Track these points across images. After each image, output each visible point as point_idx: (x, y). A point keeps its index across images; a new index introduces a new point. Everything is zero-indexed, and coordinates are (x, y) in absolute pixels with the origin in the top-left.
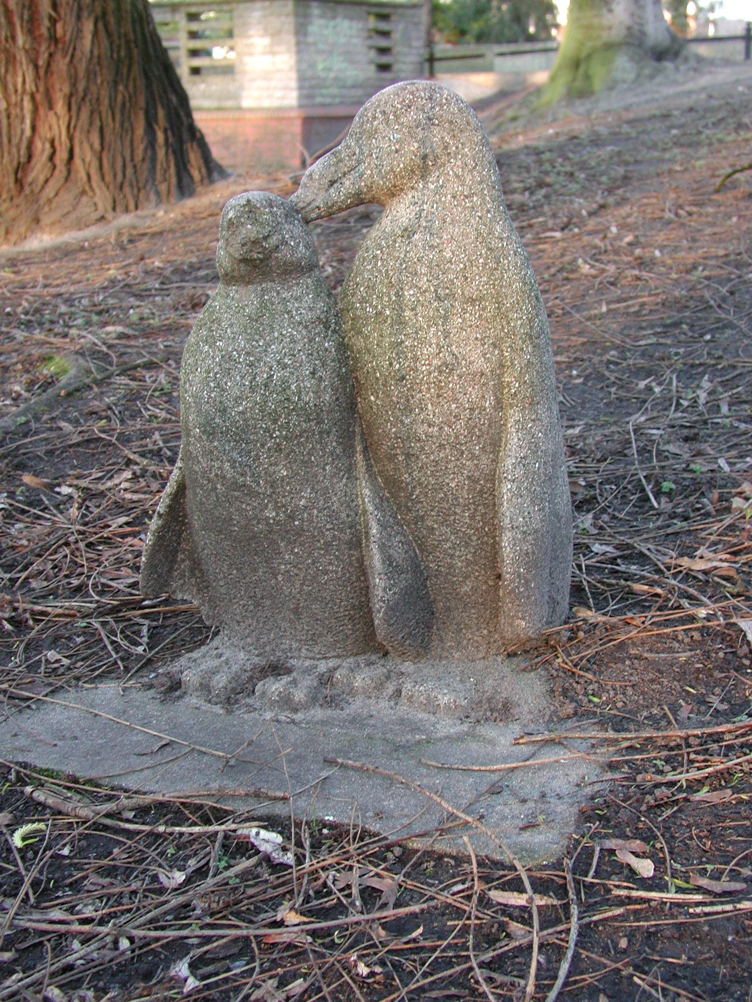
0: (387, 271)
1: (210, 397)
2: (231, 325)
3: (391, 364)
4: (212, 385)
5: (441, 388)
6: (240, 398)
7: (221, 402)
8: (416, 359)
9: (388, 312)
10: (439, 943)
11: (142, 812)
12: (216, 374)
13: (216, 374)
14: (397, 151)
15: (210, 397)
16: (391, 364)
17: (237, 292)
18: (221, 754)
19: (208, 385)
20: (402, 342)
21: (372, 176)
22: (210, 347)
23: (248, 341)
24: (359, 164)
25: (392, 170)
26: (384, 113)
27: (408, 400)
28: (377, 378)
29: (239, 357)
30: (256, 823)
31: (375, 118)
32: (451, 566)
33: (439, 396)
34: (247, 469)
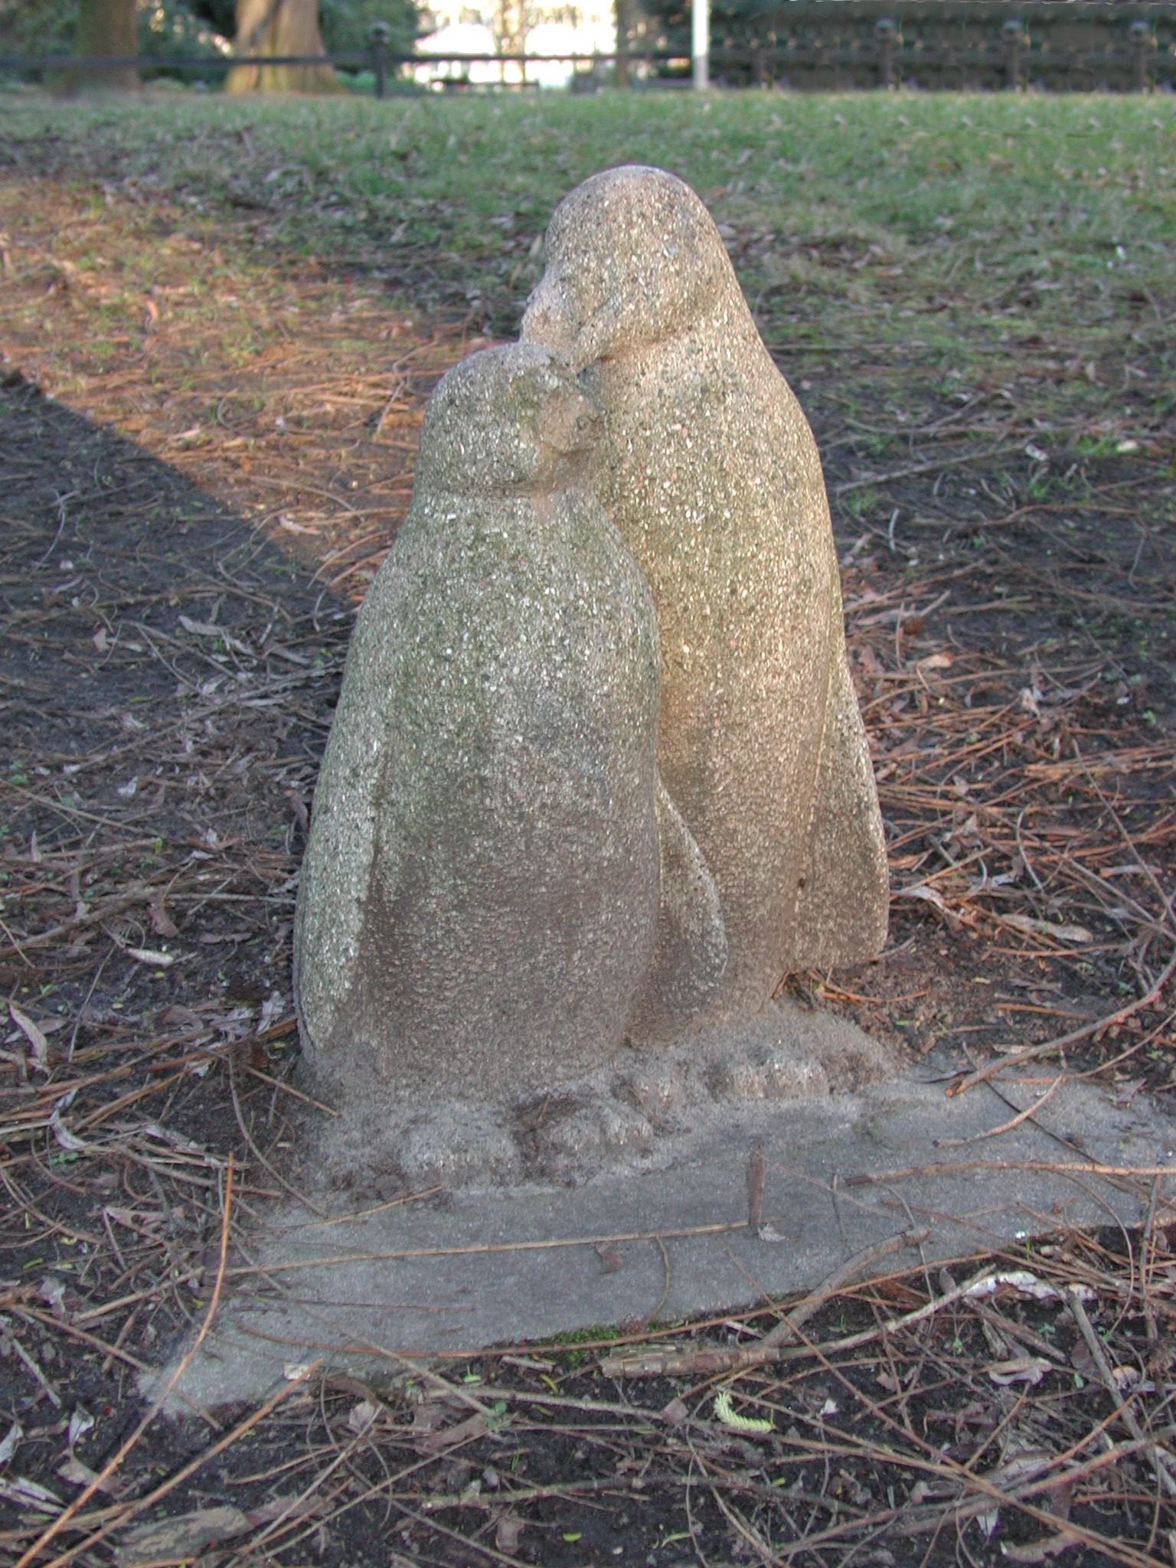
0: (709, 453)
1: (553, 678)
2: (553, 559)
3: (734, 592)
4: (558, 658)
5: (797, 617)
6: (605, 672)
7: (574, 684)
8: (770, 578)
9: (727, 514)
10: (907, 1421)
11: (822, 1321)
12: (562, 639)
13: (562, 639)
14: (678, 273)
15: (553, 678)
16: (734, 592)
17: (528, 506)
18: (716, 1227)
19: (549, 659)
20: (754, 556)
21: (636, 312)
22: (534, 598)
23: (591, 580)
24: (613, 295)
25: (672, 303)
26: (643, 215)
27: (753, 642)
28: (705, 617)
29: (591, 607)
30: (987, 1269)
31: (630, 224)
32: (749, 883)
33: (793, 628)
34: (597, 786)
